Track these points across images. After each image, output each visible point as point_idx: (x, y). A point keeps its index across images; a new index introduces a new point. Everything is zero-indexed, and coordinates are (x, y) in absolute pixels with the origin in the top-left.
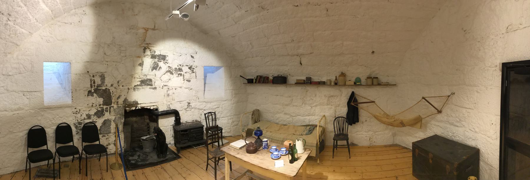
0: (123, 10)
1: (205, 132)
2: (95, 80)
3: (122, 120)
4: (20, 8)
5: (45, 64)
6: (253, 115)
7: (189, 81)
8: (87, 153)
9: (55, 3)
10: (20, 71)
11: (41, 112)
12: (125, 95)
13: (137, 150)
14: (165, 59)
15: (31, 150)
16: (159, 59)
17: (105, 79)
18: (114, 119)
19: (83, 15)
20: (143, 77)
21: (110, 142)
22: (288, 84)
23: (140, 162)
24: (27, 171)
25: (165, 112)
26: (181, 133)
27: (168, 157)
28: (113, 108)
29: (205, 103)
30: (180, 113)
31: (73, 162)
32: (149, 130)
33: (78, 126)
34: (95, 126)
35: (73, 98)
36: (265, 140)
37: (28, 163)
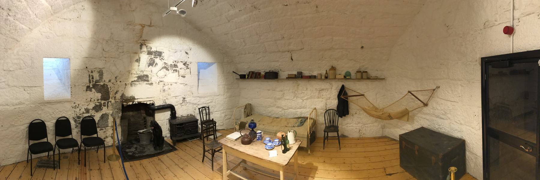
1: (200, 126)
3: (119, 115)
4: (20, 3)
5: (45, 60)
6: (245, 109)
7: (184, 77)
8: (85, 145)
10: (21, 66)
11: (41, 107)
12: (122, 91)
13: (134, 142)
14: (161, 55)
15: (32, 142)
16: (155, 55)
17: (103, 74)
18: (111, 114)
20: (140, 73)
21: (107, 135)
22: (280, 79)
26: (177, 127)
27: (164, 150)
28: (111, 103)
30: (176, 107)
31: (72, 153)
32: (145, 124)
34: (94, 120)
36: (259, 131)
37: (29, 154)
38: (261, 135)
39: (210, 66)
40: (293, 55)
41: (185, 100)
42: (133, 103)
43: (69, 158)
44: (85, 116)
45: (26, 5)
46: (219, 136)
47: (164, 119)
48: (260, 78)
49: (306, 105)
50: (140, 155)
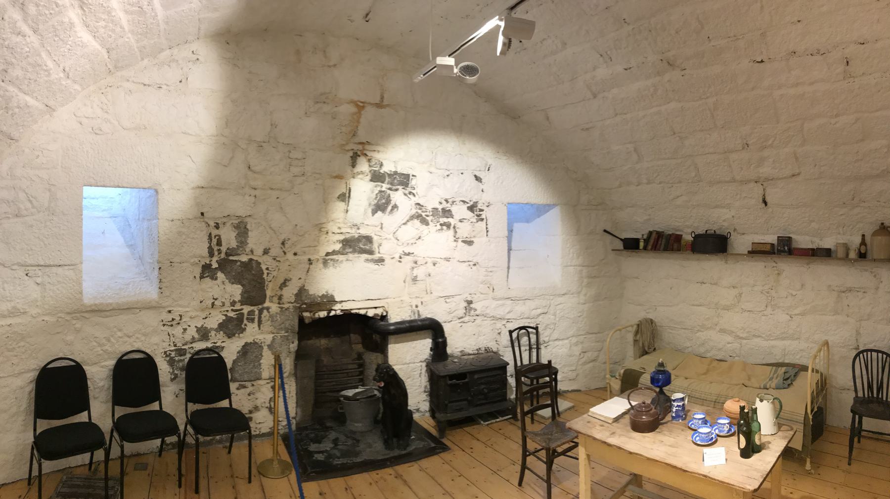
0: (298, 52)
1: (512, 381)
2: (222, 237)
3: (292, 346)
4: (19, 39)
5: (88, 191)
6: (637, 333)
7: (470, 243)
8: (197, 431)
9: (118, 29)
10: (19, 209)
11: (74, 322)
12: (300, 279)
13: (329, 424)
14: (408, 184)
15: (44, 425)
16: (392, 184)
17: (247, 234)
18: (269, 342)
19: (191, 63)
20: (349, 230)
21: (259, 403)
22: (732, 254)
23: (339, 458)
24: (32, 481)
25: (407, 325)
26: (450, 382)
27: (414, 447)
28: (269, 312)
29: (509, 302)
30: (447, 328)
31: (160, 455)
32: (361, 373)
33: (177, 359)
34: (221, 360)
35: (163, 285)
36: (679, 395)
37: (35, 462)
38: (683, 405)
39: (542, 215)
40: (768, 191)
41: (471, 309)
42: (329, 313)
43: (150, 468)
44: (196, 349)
45: (36, 44)
46: (566, 410)
47: (413, 361)
48: (679, 250)
49: (798, 330)
50: (345, 462)
